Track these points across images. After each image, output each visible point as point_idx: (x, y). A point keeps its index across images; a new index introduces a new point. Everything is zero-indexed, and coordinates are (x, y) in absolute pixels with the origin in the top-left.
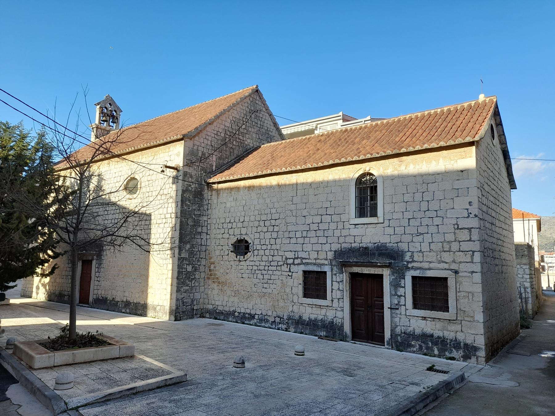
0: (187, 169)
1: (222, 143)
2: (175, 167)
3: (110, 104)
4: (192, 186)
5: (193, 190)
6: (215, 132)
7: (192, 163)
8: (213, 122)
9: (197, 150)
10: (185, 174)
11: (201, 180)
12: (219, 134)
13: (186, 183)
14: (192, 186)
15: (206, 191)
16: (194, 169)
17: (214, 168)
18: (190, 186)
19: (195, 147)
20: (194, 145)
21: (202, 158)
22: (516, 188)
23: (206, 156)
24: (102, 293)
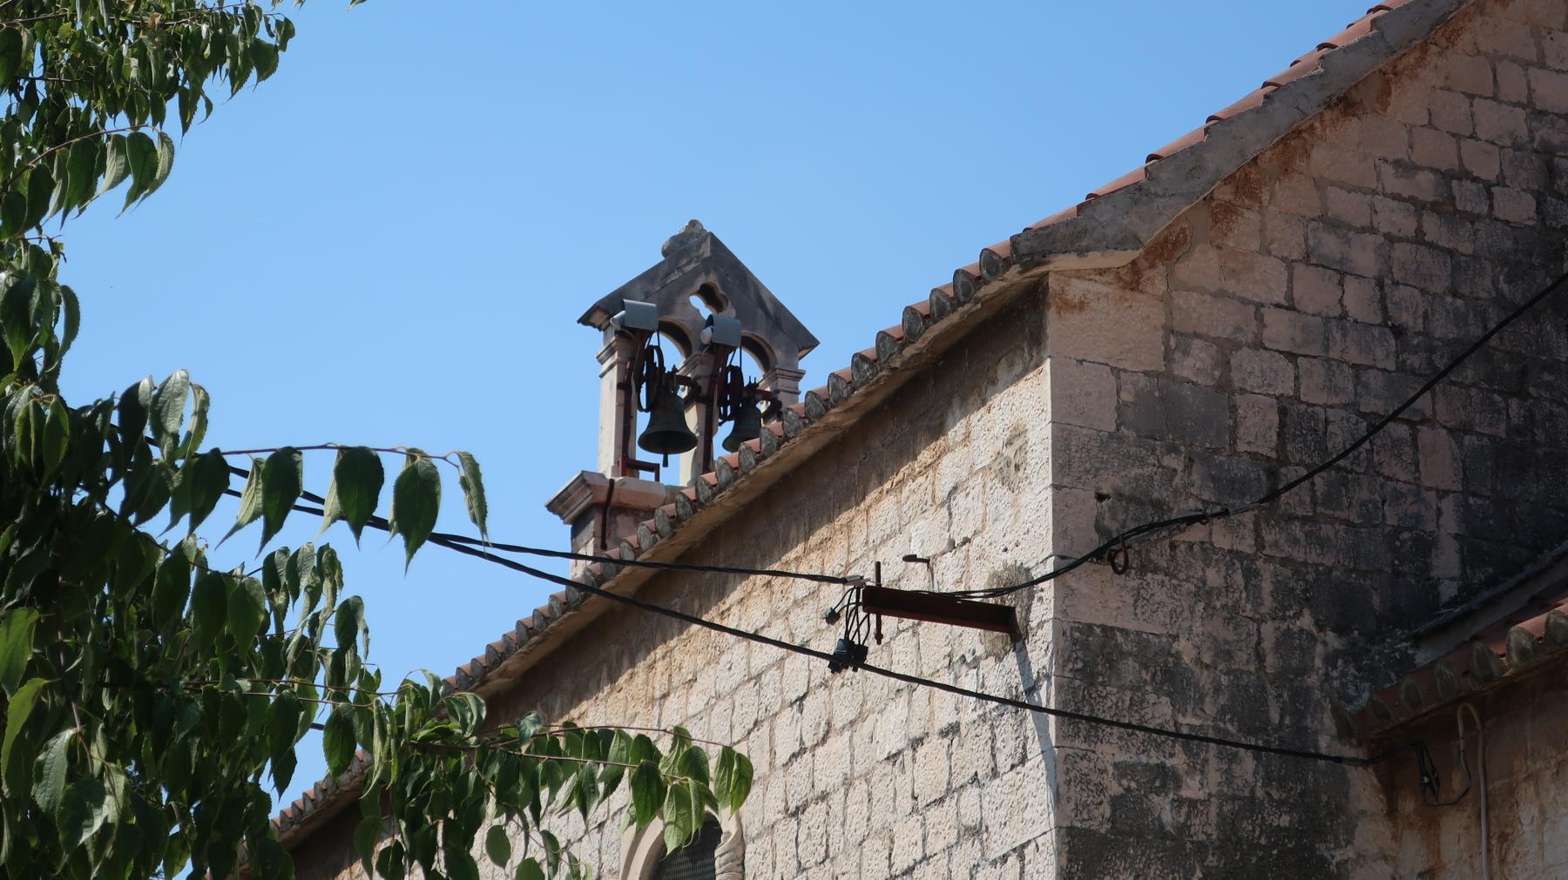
0: (1109, 601)
1: (1517, 293)
2: (752, 632)
3: (707, 293)
4: (1192, 789)
5: (1205, 828)
6: (1424, 187)
7: (1163, 524)
8: (1387, 81)
9: (1224, 386)
10: (1088, 654)
11: (1299, 703)
12: (1466, 196)
13: (1110, 751)
14: (1192, 789)
15: (1371, 833)
16: (1204, 593)
17: (1447, 563)
18: (1165, 778)
19: (1195, 365)
20: (1176, 338)
21: (1290, 473)
22: (551, 507)
23: (1338, 439)
24: (1095, 536)
